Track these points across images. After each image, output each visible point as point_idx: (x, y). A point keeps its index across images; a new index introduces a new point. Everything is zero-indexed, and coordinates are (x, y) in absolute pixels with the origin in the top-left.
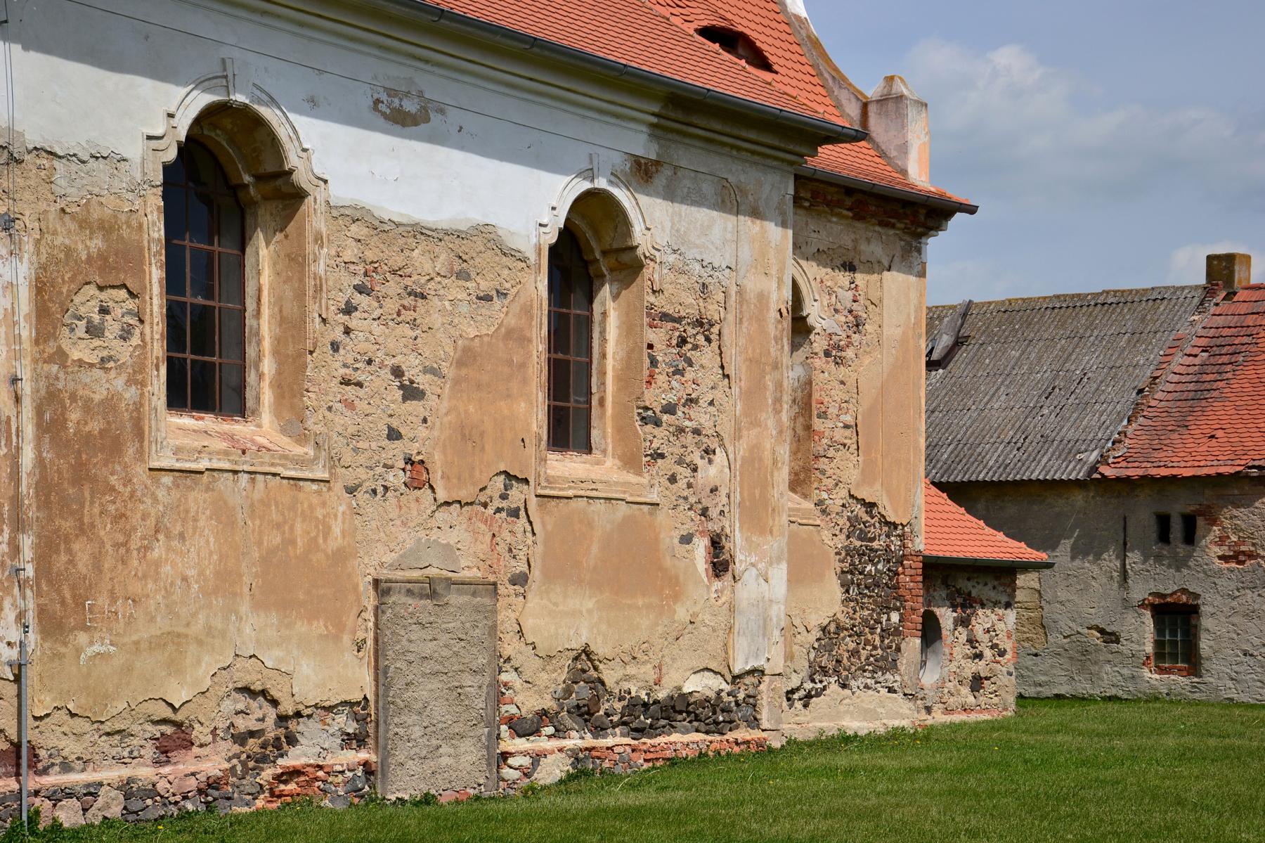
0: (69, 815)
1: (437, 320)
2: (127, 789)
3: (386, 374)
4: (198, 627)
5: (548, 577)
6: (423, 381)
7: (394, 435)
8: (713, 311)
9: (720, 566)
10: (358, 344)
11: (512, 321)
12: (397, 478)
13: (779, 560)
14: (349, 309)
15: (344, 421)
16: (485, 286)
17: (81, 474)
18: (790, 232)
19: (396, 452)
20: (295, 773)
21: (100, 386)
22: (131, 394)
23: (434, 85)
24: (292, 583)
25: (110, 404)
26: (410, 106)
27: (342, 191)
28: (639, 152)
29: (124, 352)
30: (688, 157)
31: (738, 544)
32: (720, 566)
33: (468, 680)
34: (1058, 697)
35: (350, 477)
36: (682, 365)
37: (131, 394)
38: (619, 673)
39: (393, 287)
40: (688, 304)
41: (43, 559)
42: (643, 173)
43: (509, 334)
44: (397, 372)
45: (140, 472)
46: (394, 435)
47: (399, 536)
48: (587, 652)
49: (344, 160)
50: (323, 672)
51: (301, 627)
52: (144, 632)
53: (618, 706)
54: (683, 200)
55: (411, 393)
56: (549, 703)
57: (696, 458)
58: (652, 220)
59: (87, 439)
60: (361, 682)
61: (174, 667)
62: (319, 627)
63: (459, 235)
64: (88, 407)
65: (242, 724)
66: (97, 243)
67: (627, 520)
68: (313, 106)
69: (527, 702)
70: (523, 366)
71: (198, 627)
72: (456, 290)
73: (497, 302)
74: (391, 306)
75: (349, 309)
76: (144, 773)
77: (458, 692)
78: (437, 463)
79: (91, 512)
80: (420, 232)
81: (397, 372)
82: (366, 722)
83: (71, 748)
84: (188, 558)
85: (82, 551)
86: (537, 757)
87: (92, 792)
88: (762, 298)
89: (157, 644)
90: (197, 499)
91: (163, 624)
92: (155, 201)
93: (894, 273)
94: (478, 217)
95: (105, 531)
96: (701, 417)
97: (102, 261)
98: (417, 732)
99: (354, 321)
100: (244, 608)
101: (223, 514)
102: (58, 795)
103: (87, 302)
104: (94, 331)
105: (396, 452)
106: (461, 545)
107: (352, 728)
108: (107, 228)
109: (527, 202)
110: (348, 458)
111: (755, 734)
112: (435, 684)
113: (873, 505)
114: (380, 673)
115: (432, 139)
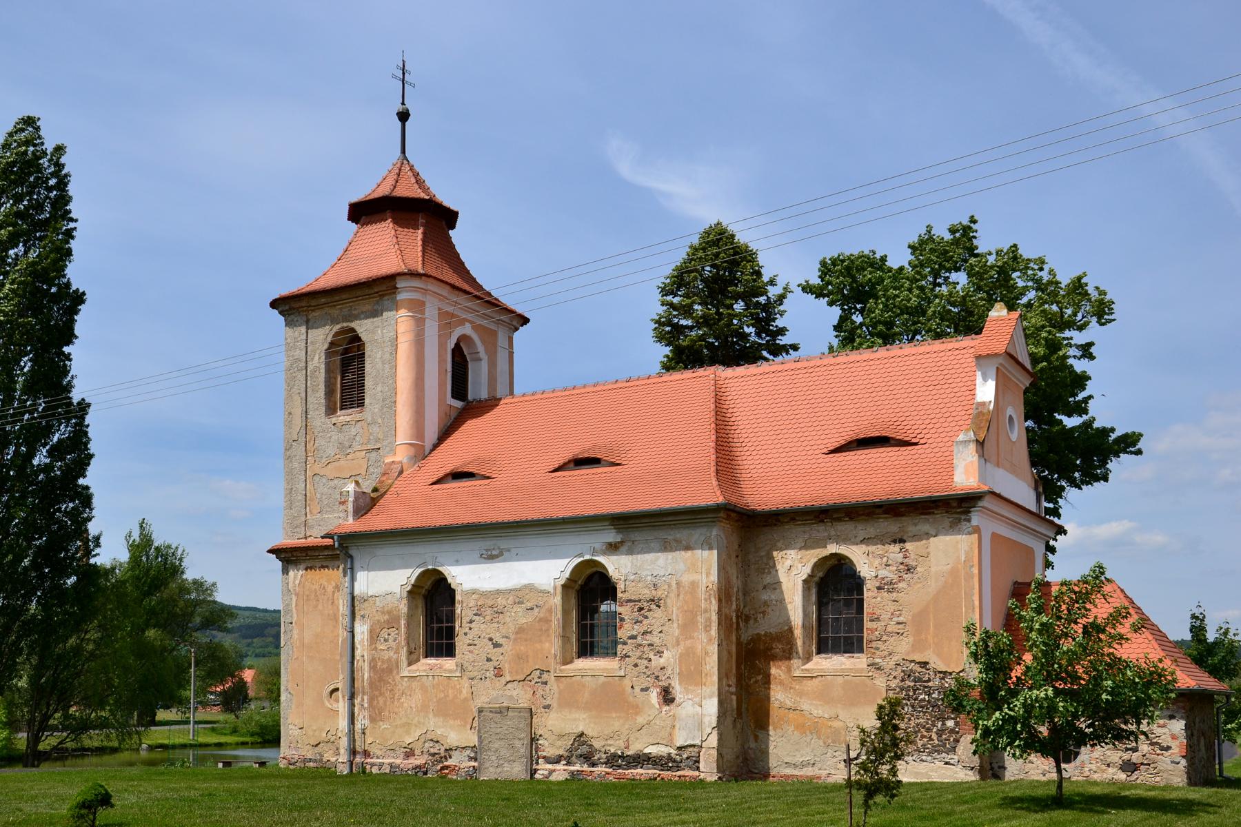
0: (375, 770)
1: (508, 620)
2: (391, 765)
3: (486, 640)
4: (415, 721)
5: (560, 706)
6: (501, 641)
7: (489, 660)
8: (659, 594)
9: (667, 697)
10: (475, 631)
11: (542, 615)
12: (490, 674)
13: (711, 697)
14: (471, 622)
15: (469, 657)
16: (529, 605)
17: (381, 680)
18: (715, 552)
19: (490, 665)
20: (447, 767)
21: (386, 655)
22: (395, 656)
23: (503, 544)
24: (445, 709)
25: (389, 660)
26: (494, 553)
27: (467, 586)
28: (611, 540)
29: (393, 645)
30: (637, 536)
31: (678, 691)
32: (667, 697)
33: (516, 742)
34: (354, 741)
35: (471, 675)
36: (641, 618)
37: (395, 656)
38: (602, 743)
39: (489, 612)
40: (647, 593)
41: (370, 702)
42: (613, 548)
43: (541, 620)
44: (491, 639)
45: (398, 678)
46: (489, 660)
47: (489, 693)
48: (582, 735)
49: (468, 576)
50: (457, 735)
51: (451, 722)
52: (398, 722)
53: (604, 756)
54: (672, 550)
55: (496, 645)
56: (561, 752)
57: (651, 656)
58: (616, 566)
59: (383, 670)
60: (474, 740)
61: (408, 733)
62: (458, 722)
63: (516, 590)
64: (383, 661)
65: (432, 751)
66: (386, 617)
67: (604, 684)
68: (457, 562)
69: (550, 751)
70: (547, 630)
71: (415, 721)
72: (518, 608)
73: (536, 610)
74: (488, 618)
75: (471, 622)
76: (398, 761)
77: (512, 746)
78: (506, 668)
79: (384, 689)
80: (498, 592)
81: (491, 639)
82: (476, 753)
83: (379, 753)
84: (412, 702)
85: (381, 700)
86: (551, 772)
87: (381, 765)
88: (694, 585)
89: (403, 725)
90: (415, 684)
91: (404, 720)
92: (405, 601)
93: (941, 538)
94: (525, 582)
95: (387, 694)
96: (655, 639)
97: (388, 622)
98: (494, 758)
99: (472, 625)
100: (431, 716)
101: (424, 689)
102: (373, 765)
103: (384, 634)
104: (386, 640)
105: (490, 665)
106: (520, 696)
107: (472, 755)
108: (389, 612)
109: (546, 572)
110: (470, 668)
111: (697, 773)
112: (502, 743)
113: (926, 663)
114: (480, 737)
115: (505, 561)
